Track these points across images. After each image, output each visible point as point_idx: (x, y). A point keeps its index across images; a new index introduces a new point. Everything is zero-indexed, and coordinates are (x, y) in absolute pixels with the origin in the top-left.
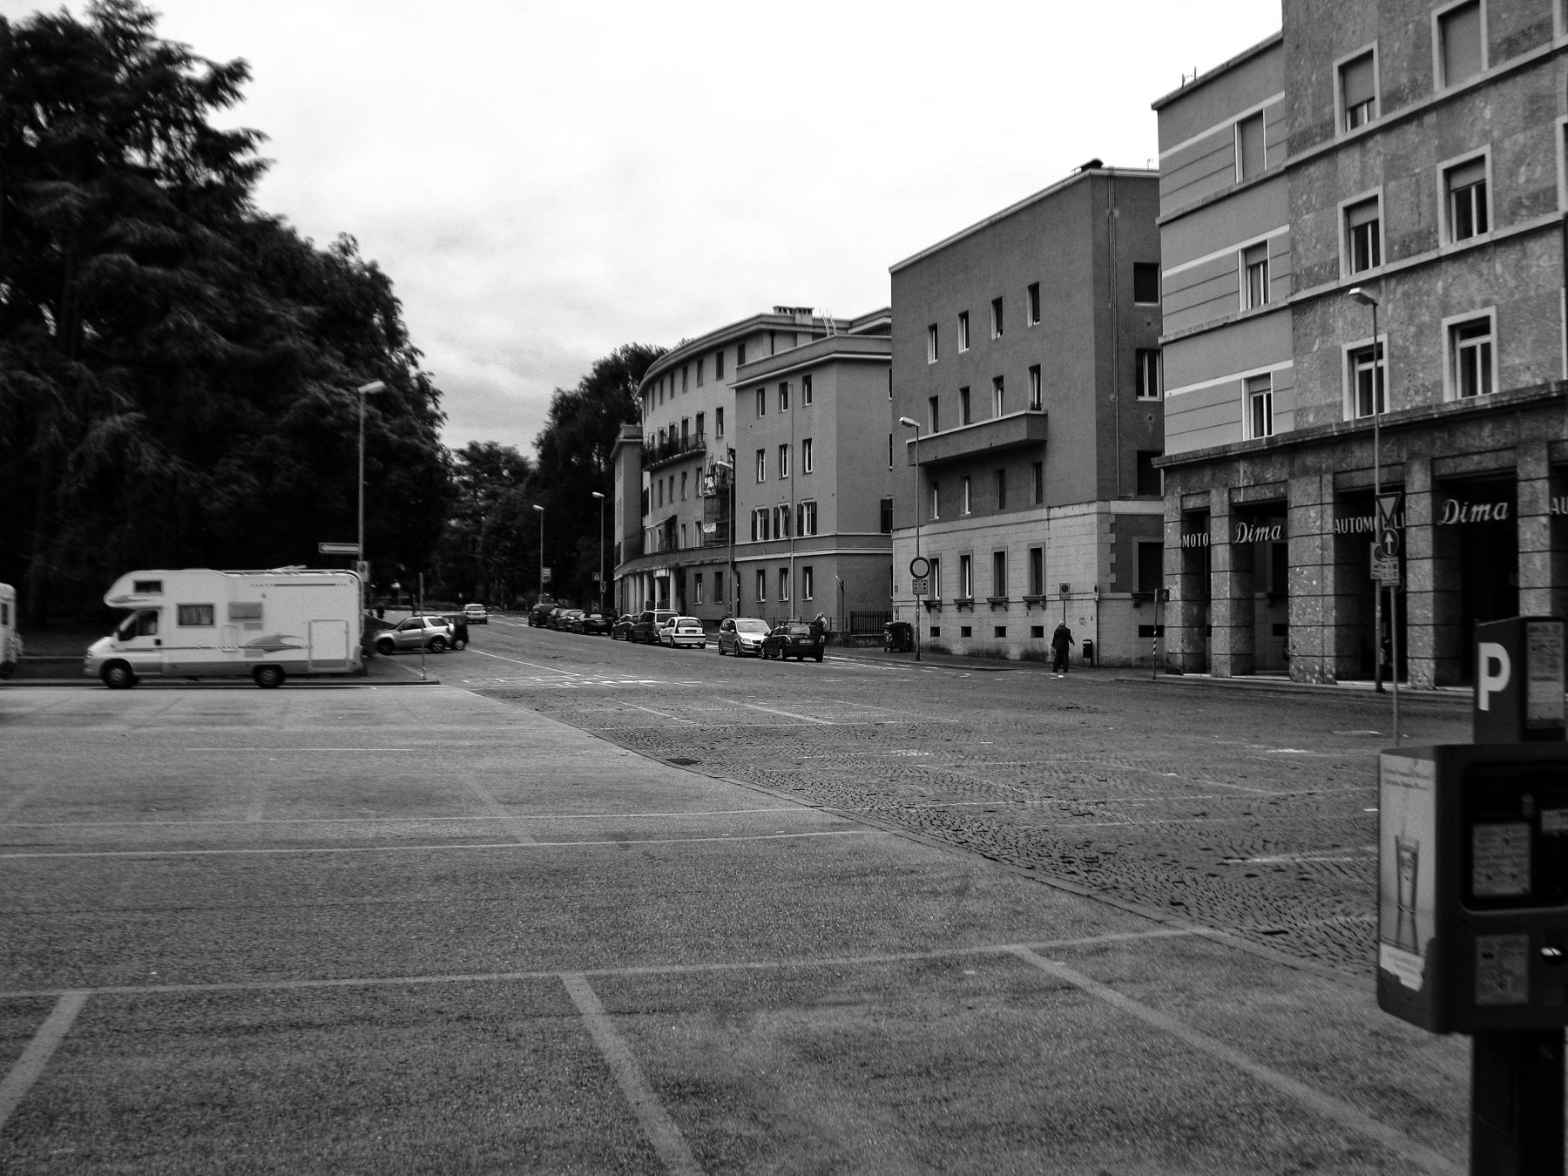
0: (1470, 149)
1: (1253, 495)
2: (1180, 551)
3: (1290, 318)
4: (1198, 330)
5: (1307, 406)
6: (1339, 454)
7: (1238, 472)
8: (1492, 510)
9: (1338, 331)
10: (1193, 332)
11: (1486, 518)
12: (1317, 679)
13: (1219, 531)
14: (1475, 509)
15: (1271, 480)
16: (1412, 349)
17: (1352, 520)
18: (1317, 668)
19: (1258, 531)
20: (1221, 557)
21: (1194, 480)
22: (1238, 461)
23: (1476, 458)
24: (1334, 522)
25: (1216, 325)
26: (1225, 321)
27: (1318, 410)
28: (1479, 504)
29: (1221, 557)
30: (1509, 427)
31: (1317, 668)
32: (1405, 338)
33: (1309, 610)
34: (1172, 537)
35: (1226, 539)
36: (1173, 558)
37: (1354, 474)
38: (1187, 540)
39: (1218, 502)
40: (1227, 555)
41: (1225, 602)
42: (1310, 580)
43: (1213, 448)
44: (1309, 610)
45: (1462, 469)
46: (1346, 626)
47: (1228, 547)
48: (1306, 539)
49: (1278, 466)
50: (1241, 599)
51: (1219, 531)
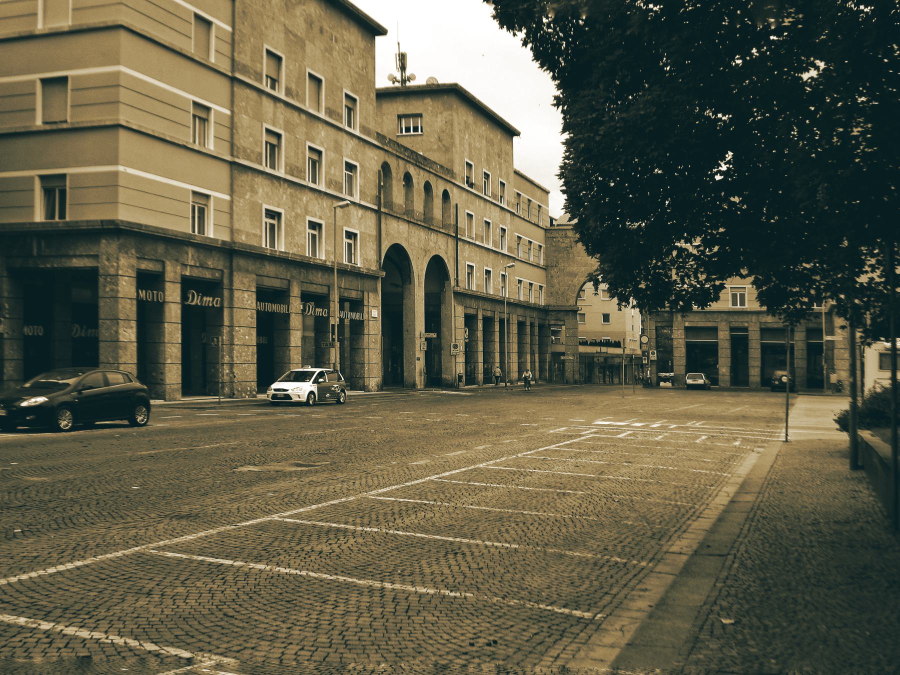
0: (262, 70)
1: (196, 273)
2: (135, 302)
3: (705, 528)
4: (161, 136)
5: (242, 229)
6: (258, 264)
7: (187, 254)
8: (213, 301)
9: (260, 195)
10: (156, 135)
11: (211, 305)
12: (249, 395)
13: (173, 293)
14: (205, 299)
15: (211, 266)
16: (293, 223)
17: (155, 292)
18: (249, 389)
19: (317, 310)
20: (173, 312)
21: (148, 248)
22: (187, 245)
23: (315, 286)
24: (257, 303)
25: (176, 141)
26: (185, 144)
27: (248, 235)
28: (207, 296)
29: (173, 312)
30: (326, 277)
31: (249, 389)
32: (290, 216)
33: (244, 354)
34: (127, 289)
35: (178, 299)
36: (128, 306)
37: (264, 278)
38: (262, 306)
39: (172, 272)
40: (179, 312)
41: (177, 345)
42: (244, 336)
43: (183, 233)
44: (244, 354)
45: (309, 290)
46: (160, 384)
47: (180, 306)
48: (242, 310)
49: (216, 258)
50: (18, 359)
51: (173, 293)
